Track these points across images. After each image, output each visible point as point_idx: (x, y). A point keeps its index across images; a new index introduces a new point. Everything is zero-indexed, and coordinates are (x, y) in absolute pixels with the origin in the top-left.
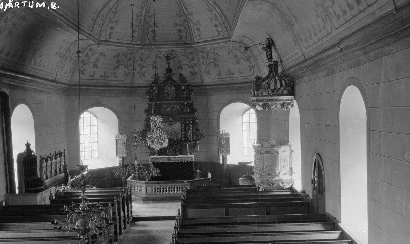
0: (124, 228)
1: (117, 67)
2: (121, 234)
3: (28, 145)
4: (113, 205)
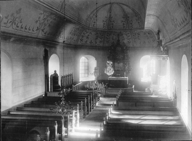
0: (93, 108)
1: (96, 39)
2: (90, 111)
3: (55, 71)
4: (87, 99)
